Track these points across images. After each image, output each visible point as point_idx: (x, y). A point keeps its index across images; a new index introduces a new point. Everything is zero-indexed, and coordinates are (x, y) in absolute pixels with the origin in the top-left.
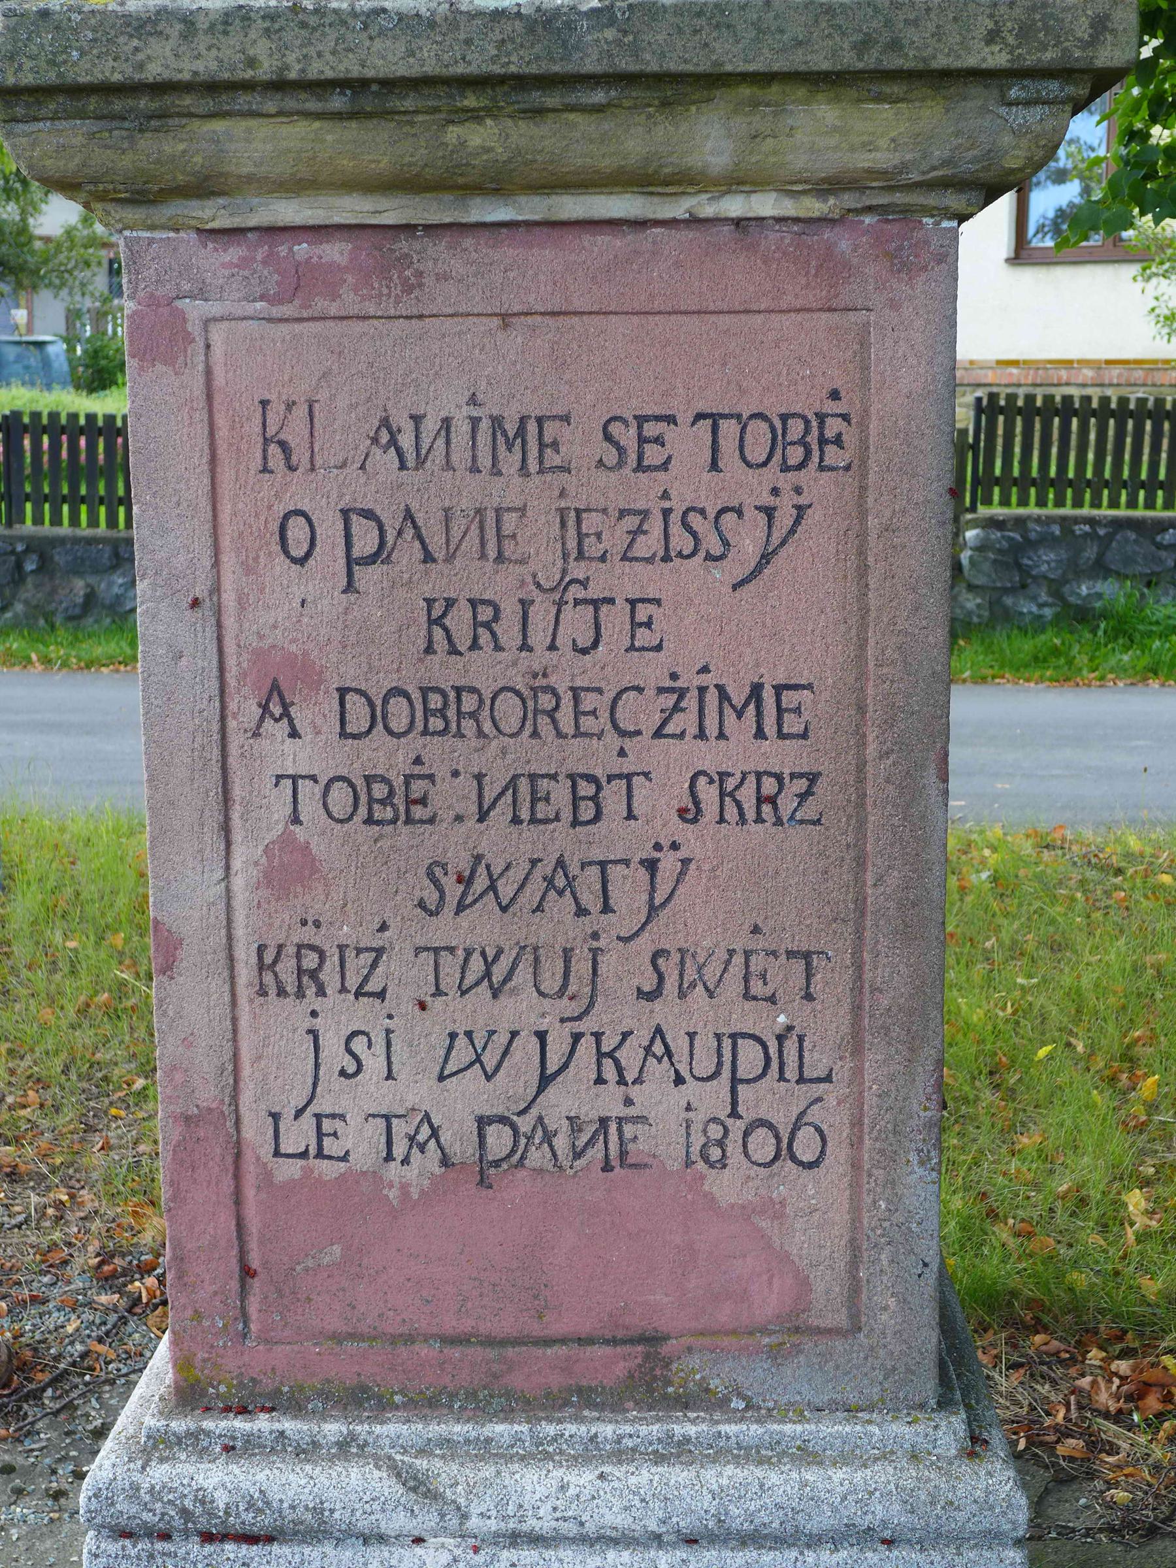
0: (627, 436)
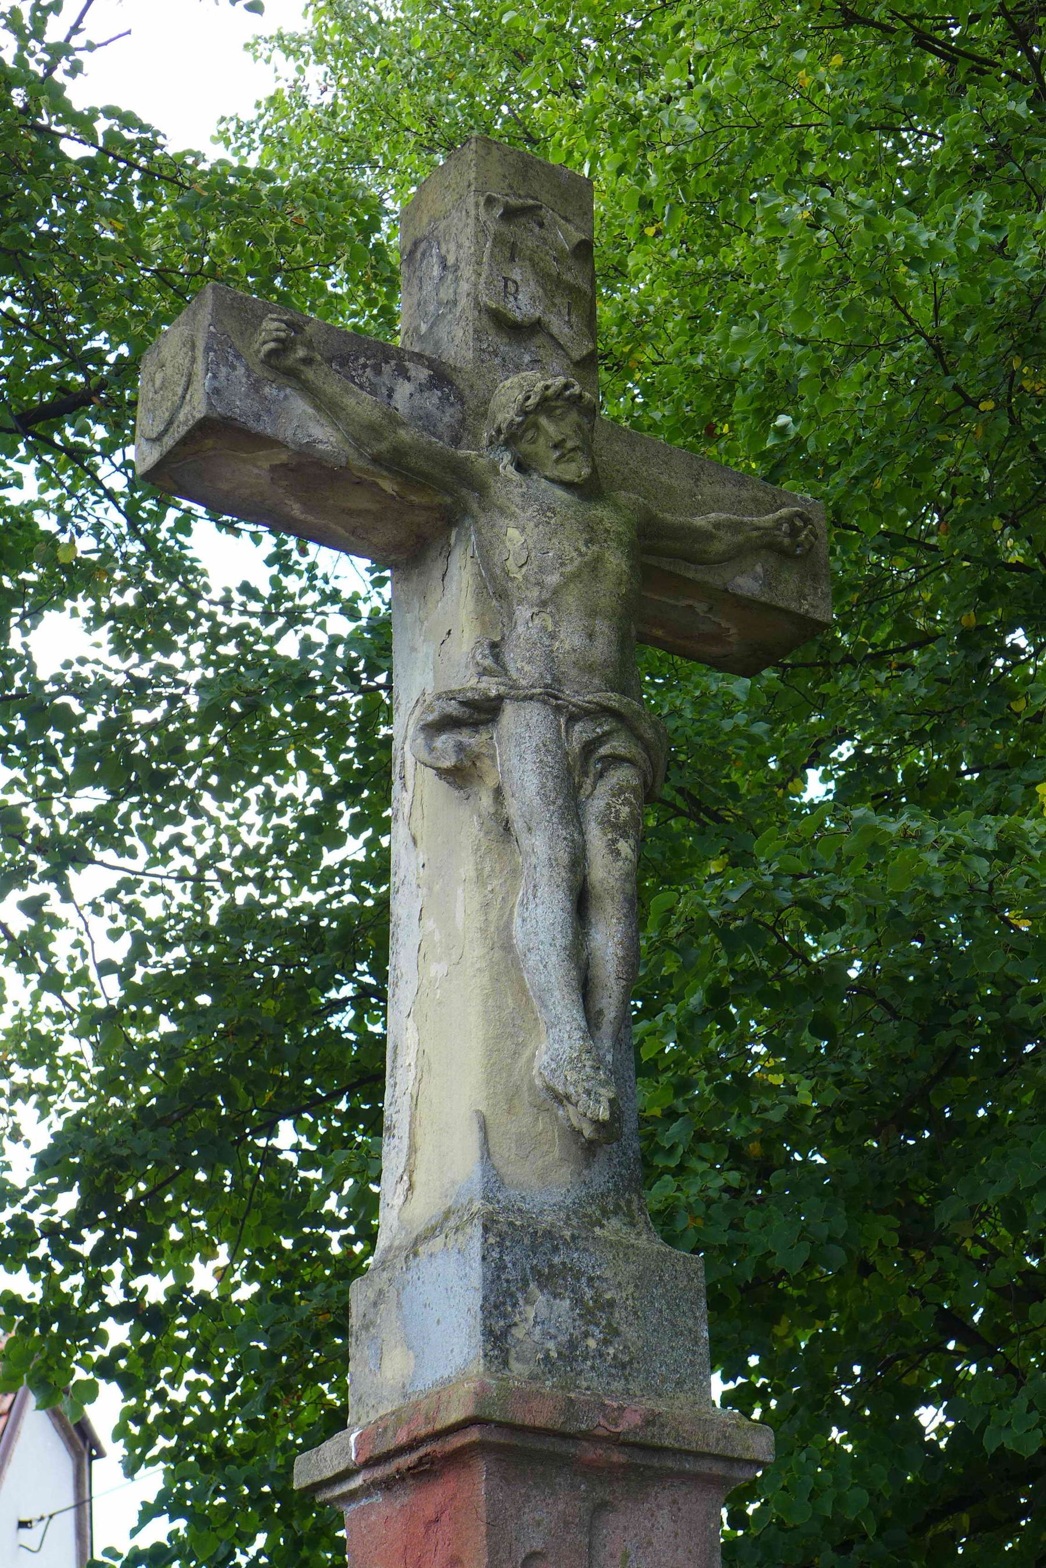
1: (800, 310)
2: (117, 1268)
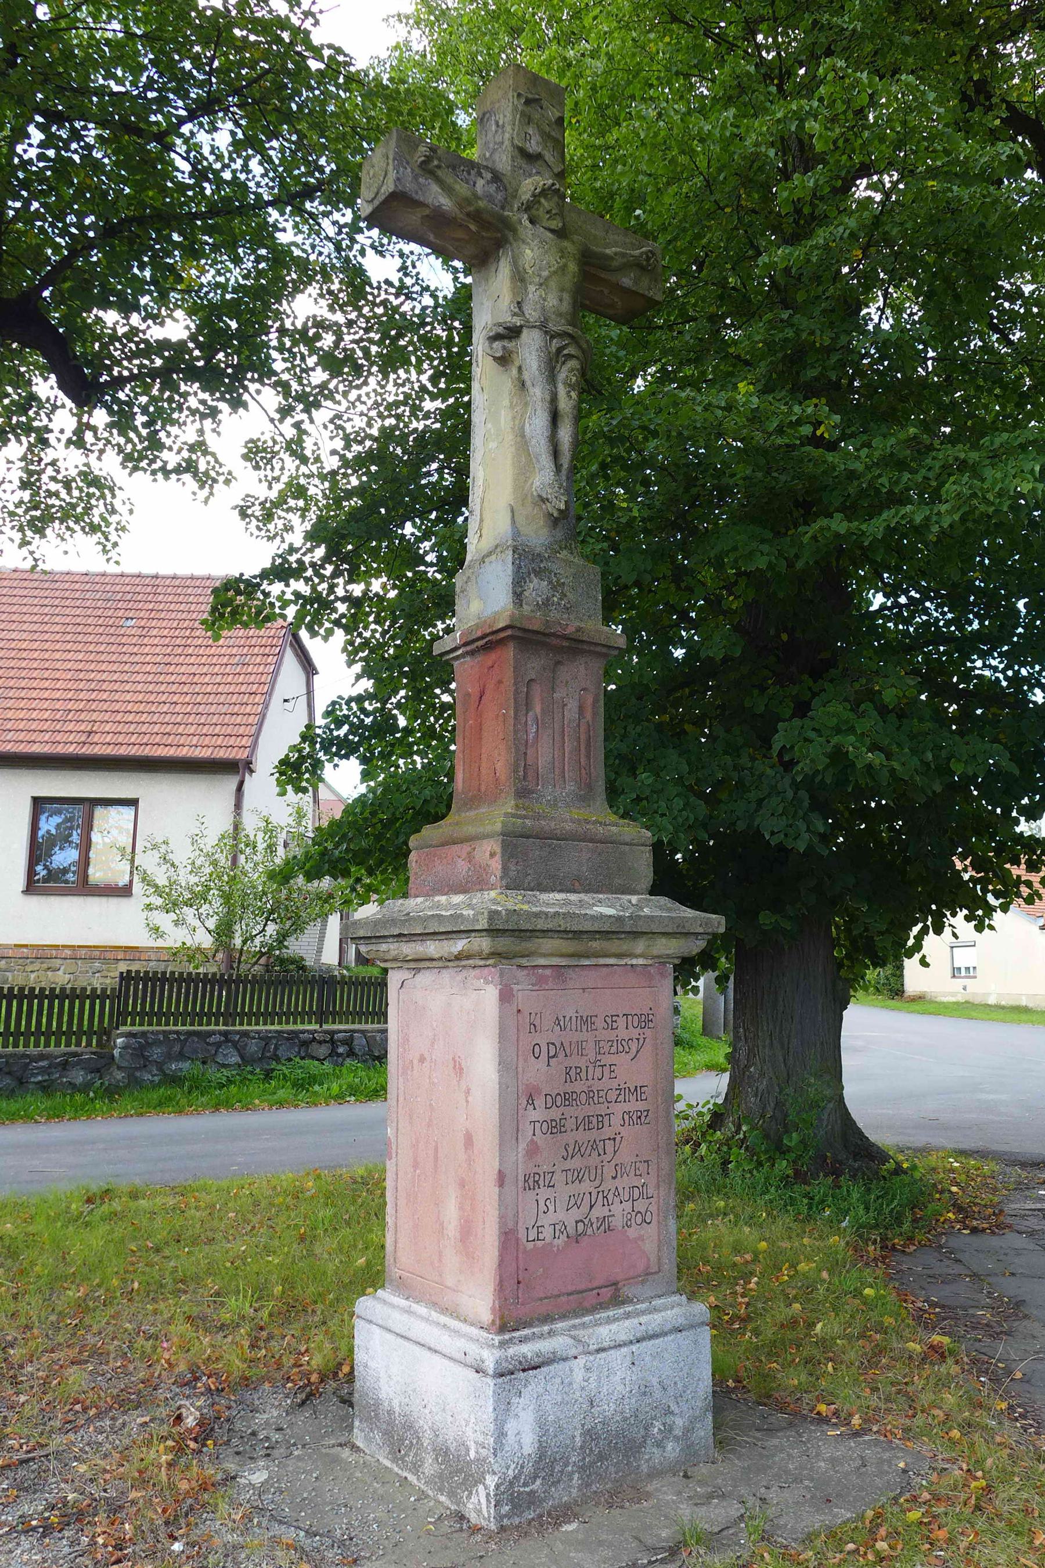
0: (609, 1020)
1: (650, 159)
2: (340, 581)
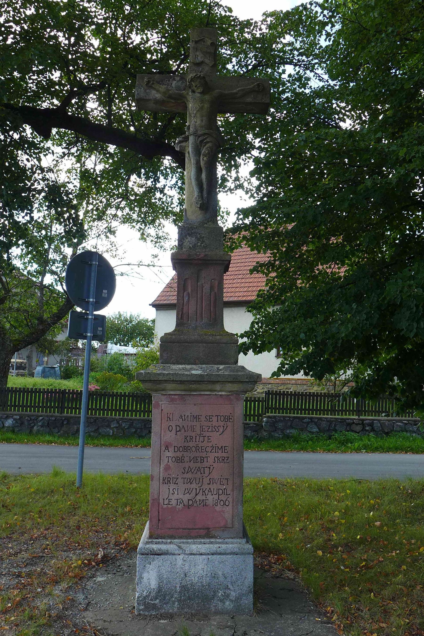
0: (208, 418)
